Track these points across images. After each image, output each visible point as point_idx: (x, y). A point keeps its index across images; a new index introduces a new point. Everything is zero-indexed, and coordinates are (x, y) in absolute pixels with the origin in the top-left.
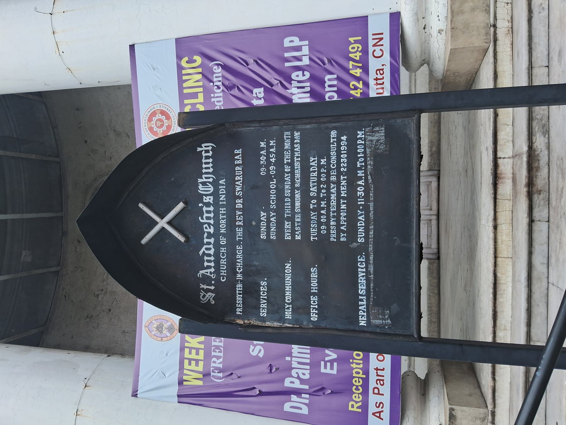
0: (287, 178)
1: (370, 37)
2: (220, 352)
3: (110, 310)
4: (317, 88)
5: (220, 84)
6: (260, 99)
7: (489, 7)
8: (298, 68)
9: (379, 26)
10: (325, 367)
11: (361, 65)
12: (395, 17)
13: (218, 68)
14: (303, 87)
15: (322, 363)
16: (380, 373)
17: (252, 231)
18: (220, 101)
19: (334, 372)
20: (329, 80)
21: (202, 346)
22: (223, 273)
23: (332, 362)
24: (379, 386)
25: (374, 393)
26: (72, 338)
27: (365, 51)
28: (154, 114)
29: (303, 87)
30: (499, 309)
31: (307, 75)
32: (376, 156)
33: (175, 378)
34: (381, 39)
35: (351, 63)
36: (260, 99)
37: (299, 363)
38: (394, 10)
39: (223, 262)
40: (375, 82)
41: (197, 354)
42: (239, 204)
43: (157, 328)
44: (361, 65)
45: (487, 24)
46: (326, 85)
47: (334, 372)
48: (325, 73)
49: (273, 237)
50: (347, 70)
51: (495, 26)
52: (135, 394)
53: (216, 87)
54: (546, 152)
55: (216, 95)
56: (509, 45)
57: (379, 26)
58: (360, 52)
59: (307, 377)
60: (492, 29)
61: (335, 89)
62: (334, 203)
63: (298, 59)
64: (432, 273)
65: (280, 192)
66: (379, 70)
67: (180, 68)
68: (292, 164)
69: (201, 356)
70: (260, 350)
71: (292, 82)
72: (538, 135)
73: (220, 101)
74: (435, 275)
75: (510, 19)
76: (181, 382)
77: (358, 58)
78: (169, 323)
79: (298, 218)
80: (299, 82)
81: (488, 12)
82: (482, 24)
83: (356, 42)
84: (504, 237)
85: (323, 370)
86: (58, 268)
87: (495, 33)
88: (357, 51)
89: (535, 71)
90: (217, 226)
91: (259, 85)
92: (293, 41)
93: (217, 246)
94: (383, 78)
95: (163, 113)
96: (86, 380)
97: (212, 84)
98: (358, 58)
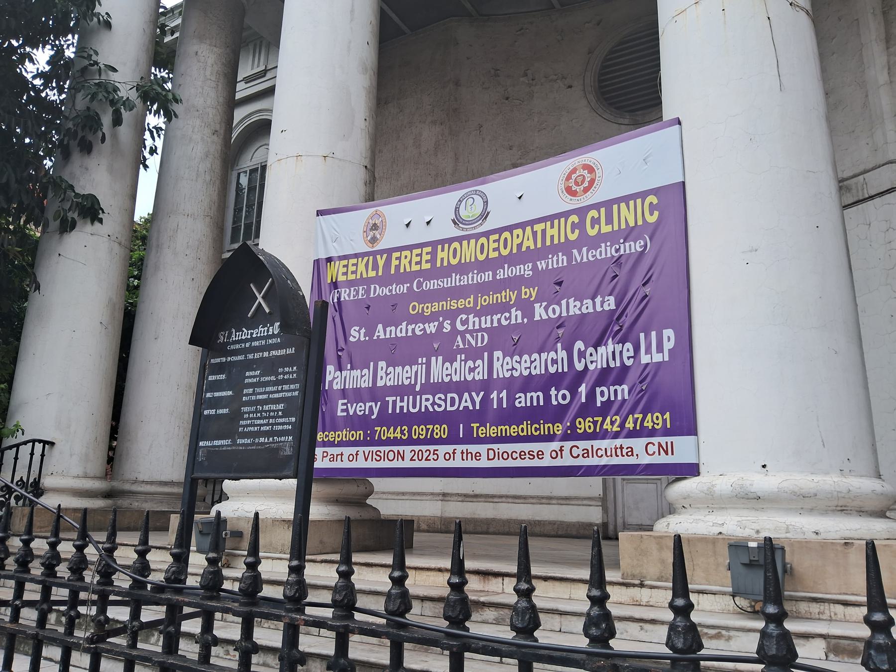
0: (275, 389)
1: (669, 439)
2: (354, 296)
3: (507, 99)
4: (613, 375)
5: (622, 252)
6: (602, 306)
7: (665, 581)
8: (637, 349)
9: (682, 449)
10: (343, 404)
11: (638, 428)
12: (692, 470)
13: (641, 247)
14: (614, 359)
15: (346, 401)
16: (339, 457)
17: (249, 365)
18: (601, 255)
19: (339, 414)
20: (623, 390)
21: (358, 277)
22: (233, 347)
23: (347, 410)
24: (329, 457)
25: (488, 450)
26: (468, 58)
27: (652, 433)
28: (591, 169)
29: (614, 359)
30: (374, 569)
31: (629, 363)
32: (277, 450)
33: (334, 254)
34: (667, 454)
35: (641, 416)
36: (602, 306)
37: (345, 378)
38: (702, 469)
39: (238, 346)
40: (618, 446)
41: (353, 273)
42: (266, 354)
43: (375, 224)
44: (638, 428)
45: (644, 577)
46: (617, 387)
47: (339, 414)
48: (631, 385)
49: (247, 381)
50: (632, 411)
51: (642, 585)
52: (320, 213)
53: (618, 247)
54: (479, 620)
55: (608, 248)
56: (620, 600)
57: (682, 449)
58: (653, 427)
59: (335, 387)
60: (637, 582)
61: (612, 398)
62: (259, 422)
63: (648, 351)
64: (585, 529)
65: (267, 384)
66: (632, 451)
67: (643, 195)
68: (282, 391)
69: (351, 277)
70: (355, 337)
71: (621, 345)
72: (495, 613)
73: (601, 255)
74: (582, 532)
75: (651, 604)
76: (329, 260)
77: (645, 424)
78: (378, 236)
79: (253, 398)
80: (621, 352)
81: (659, 580)
82: (645, 571)
83: (664, 421)
84: (432, 578)
85: (341, 402)
86: (558, 6)
87: (634, 585)
88: (654, 423)
89: (557, 618)
90: (257, 339)
91: (618, 305)
92: (669, 340)
93: (246, 340)
94: (623, 456)
95: (592, 182)
96: (331, 155)
97: (622, 241)
98: (645, 424)
